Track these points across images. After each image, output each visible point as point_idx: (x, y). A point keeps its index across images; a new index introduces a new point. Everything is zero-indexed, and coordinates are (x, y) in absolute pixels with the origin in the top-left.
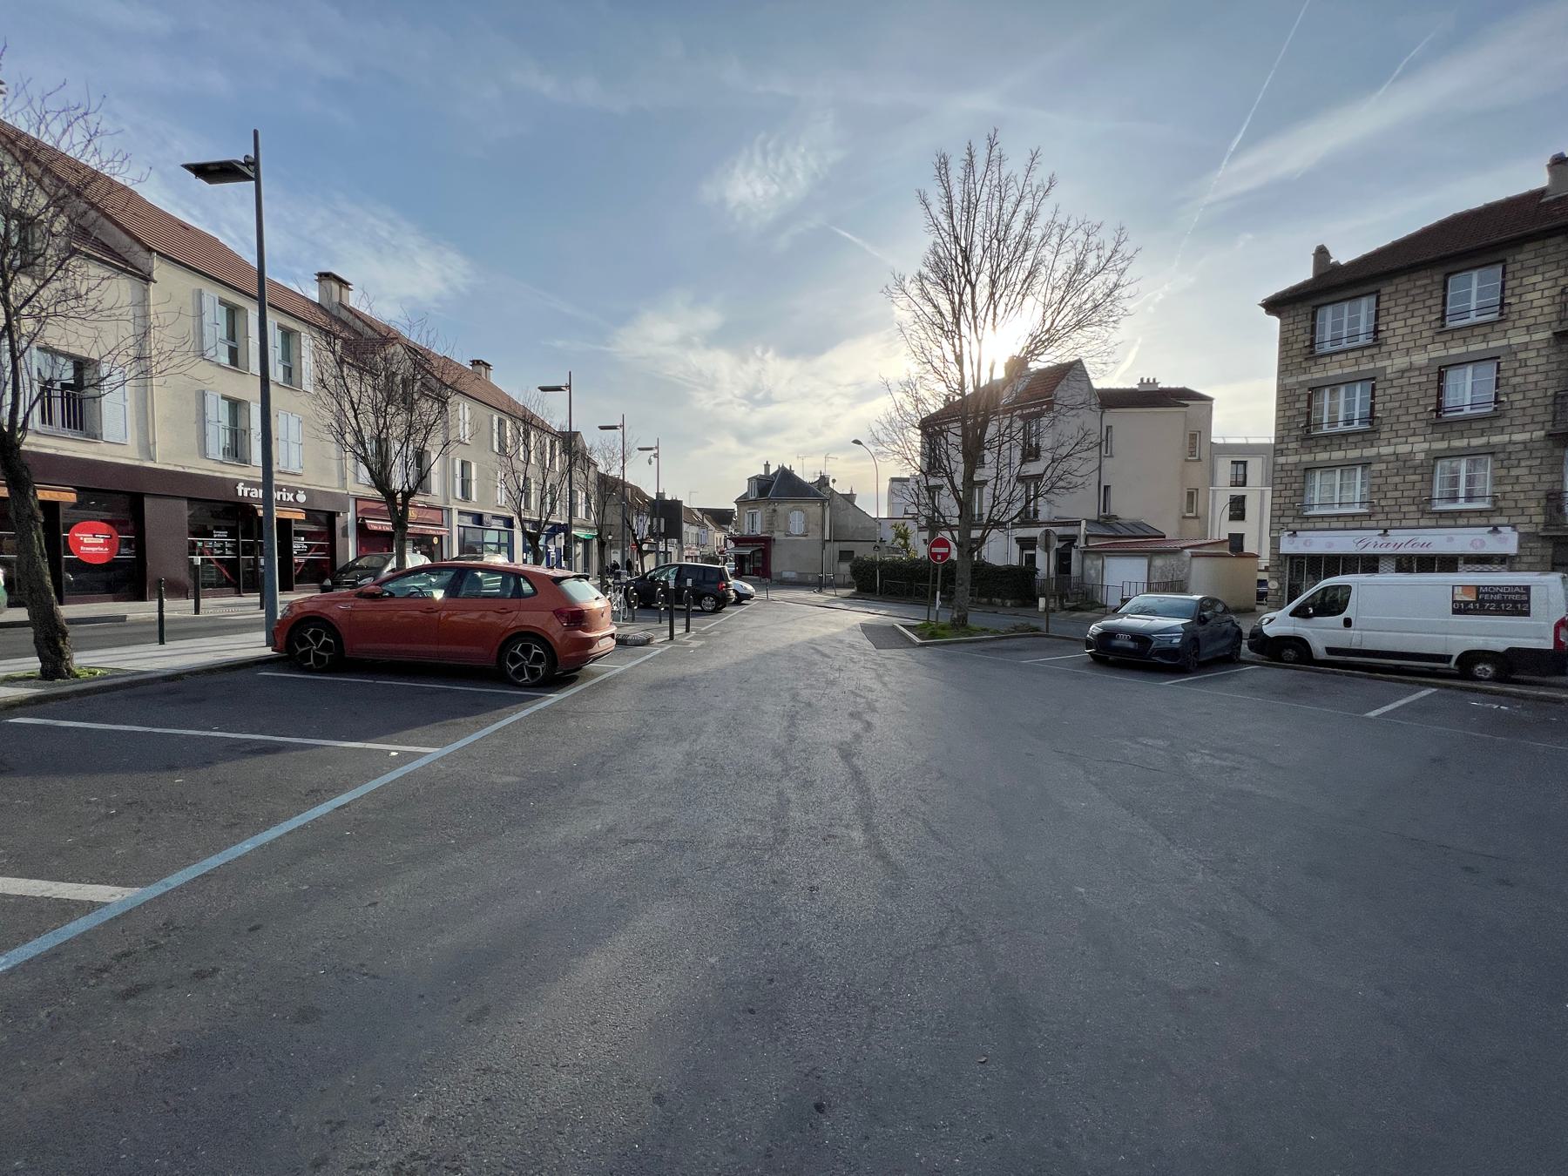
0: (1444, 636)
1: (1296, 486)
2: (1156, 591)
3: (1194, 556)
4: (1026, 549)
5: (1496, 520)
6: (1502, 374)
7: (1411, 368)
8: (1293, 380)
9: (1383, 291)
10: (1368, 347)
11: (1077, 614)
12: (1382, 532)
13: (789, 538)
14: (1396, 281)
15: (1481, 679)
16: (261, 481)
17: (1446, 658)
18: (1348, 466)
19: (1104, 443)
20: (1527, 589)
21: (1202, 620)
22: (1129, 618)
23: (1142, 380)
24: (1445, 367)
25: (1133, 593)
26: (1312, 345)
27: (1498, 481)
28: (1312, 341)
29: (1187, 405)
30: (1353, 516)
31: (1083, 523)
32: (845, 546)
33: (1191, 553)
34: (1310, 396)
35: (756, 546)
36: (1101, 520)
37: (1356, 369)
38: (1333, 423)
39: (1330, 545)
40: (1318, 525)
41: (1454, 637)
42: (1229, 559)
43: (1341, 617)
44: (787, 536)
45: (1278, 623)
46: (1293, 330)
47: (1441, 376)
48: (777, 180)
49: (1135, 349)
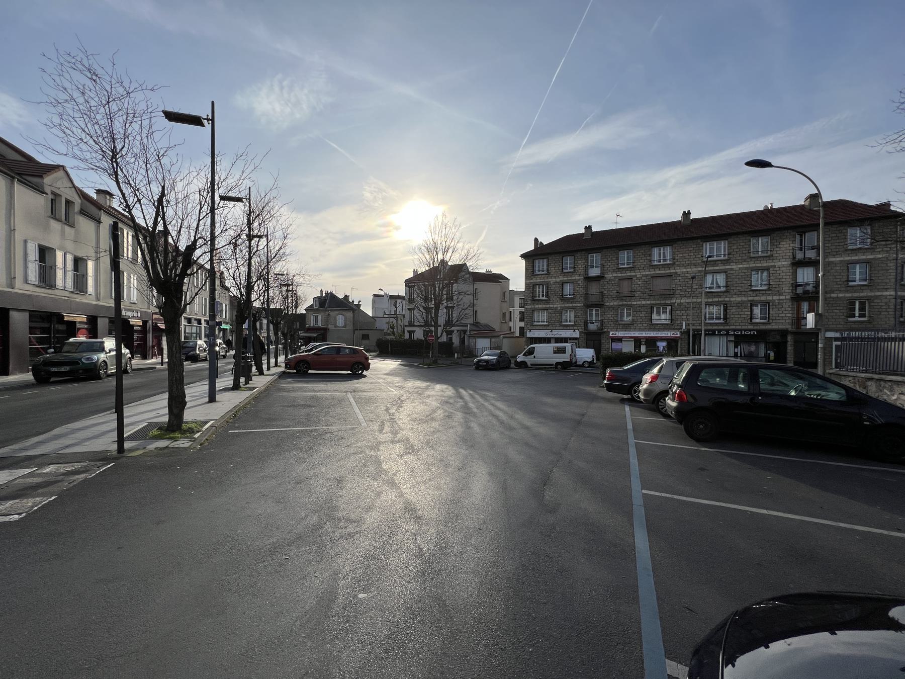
1: (530, 315)
3: (503, 338)
5: (575, 328)
8: (529, 281)
10: (547, 274)
16: (114, 306)
17: (552, 365)
19: (475, 294)
21: (501, 357)
25: (485, 350)
29: (501, 282)
31: (469, 325)
32: (365, 332)
38: (539, 296)
39: (539, 335)
43: (533, 356)
45: (521, 358)
48: (290, 105)
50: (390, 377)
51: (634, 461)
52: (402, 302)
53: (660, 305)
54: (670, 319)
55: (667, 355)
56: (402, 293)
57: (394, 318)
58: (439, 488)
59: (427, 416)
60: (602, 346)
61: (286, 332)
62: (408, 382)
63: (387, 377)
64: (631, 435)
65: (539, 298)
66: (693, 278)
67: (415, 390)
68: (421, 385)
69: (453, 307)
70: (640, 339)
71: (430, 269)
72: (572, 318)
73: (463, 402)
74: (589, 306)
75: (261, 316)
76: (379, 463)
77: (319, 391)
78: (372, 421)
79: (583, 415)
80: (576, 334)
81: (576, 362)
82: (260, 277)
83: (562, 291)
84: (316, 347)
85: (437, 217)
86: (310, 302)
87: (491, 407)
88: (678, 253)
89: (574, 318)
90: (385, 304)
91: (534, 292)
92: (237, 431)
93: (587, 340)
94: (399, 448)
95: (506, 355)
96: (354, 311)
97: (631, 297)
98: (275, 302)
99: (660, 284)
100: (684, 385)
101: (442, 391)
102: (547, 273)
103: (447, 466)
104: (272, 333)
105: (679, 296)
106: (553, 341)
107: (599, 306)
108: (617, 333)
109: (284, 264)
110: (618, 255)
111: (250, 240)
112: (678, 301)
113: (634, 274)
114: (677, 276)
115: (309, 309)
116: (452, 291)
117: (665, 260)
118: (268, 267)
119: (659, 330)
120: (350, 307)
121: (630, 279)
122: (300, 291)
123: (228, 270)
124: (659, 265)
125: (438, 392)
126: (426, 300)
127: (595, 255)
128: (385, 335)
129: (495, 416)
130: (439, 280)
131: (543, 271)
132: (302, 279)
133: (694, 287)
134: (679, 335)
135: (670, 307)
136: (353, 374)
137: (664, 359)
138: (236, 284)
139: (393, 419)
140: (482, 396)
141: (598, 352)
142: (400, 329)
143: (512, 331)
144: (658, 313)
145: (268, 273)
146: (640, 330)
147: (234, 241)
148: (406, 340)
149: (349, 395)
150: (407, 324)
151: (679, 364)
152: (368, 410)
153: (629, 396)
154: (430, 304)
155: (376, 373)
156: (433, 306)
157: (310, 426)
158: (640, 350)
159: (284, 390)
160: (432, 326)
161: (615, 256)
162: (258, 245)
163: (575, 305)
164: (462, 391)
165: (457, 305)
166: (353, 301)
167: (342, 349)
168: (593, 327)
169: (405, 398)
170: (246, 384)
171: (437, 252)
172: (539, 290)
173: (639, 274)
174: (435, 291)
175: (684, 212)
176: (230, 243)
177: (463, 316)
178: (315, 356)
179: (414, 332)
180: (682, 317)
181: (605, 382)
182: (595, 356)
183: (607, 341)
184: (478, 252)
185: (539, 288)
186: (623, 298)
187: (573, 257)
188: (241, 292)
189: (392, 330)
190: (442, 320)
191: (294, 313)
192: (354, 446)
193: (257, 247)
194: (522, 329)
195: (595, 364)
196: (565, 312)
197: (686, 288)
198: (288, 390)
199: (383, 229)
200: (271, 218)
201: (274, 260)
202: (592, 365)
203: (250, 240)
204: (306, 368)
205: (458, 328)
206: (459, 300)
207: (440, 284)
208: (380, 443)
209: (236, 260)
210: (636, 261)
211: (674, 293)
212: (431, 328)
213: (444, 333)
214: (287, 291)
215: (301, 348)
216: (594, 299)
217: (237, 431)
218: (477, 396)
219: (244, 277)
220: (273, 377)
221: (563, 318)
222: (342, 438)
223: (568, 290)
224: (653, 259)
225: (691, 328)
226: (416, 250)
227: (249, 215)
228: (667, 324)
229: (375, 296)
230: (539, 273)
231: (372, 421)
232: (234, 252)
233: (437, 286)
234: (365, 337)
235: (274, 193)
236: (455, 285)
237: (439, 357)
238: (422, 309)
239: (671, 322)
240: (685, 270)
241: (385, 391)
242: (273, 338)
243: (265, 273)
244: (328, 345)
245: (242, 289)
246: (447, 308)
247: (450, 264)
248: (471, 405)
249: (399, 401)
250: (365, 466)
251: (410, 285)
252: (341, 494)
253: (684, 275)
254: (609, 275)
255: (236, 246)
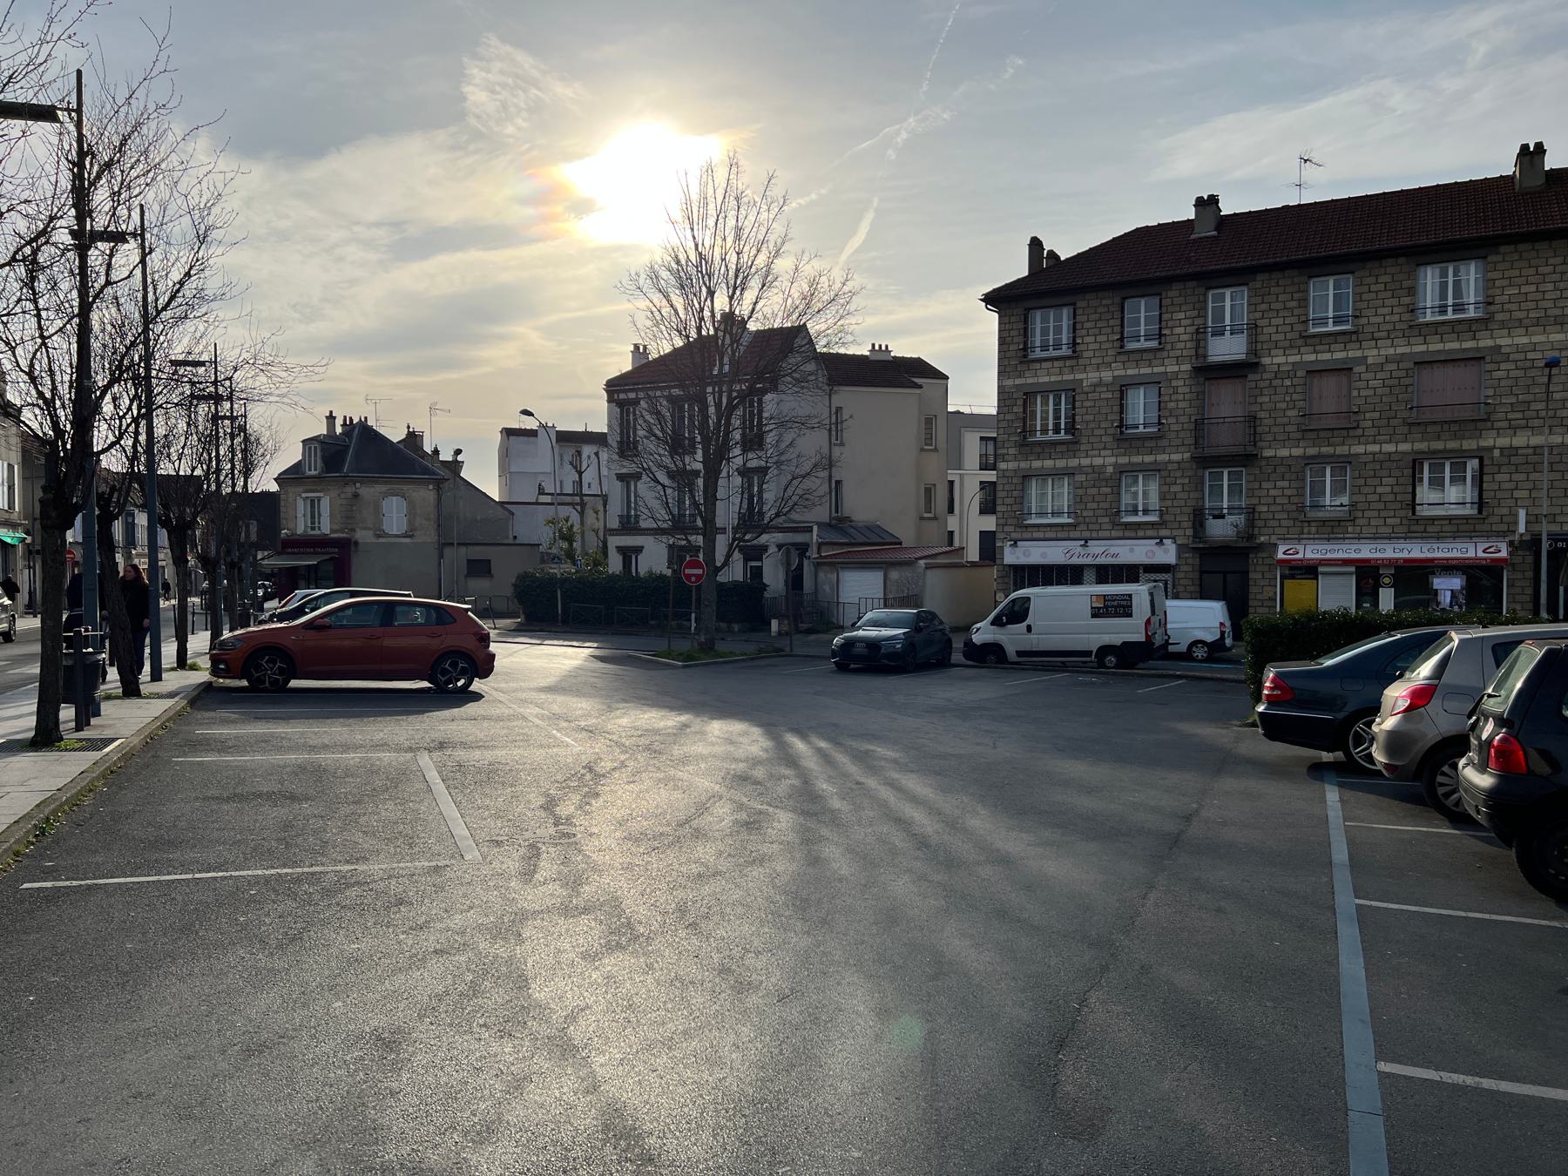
0: (1087, 636)
1: (1015, 493)
2: (892, 607)
3: (928, 567)
4: (751, 560)
5: (1164, 532)
6: (1162, 399)
7: (1100, 384)
9: (1080, 304)
11: (813, 637)
12: (1083, 542)
13: (384, 540)
14: (1088, 296)
15: (1109, 668)
17: (1088, 653)
18: (1057, 474)
19: (836, 426)
20: (1130, 596)
21: (918, 630)
22: (864, 630)
23: (873, 345)
24: (1124, 386)
25: (869, 607)
26: (1025, 349)
27: (1163, 497)
28: (1025, 343)
29: (920, 387)
30: (1062, 525)
31: (815, 528)
32: (478, 553)
33: (925, 564)
34: (1025, 401)
35: (323, 553)
36: (833, 522)
37: (1059, 378)
38: (1045, 431)
39: (1044, 555)
40: (1036, 535)
41: (1093, 636)
42: (964, 569)
43: (1025, 624)
44: (379, 536)
45: (983, 633)
46: (1009, 330)
47: (1122, 392)
49: (870, 216)
50: (560, 698)
51: (1352, 967)
52: (597, 454)
53: (1446, 454)
54: (1476, 500)
55: (1464, 620)
56: (600, 425)
57: (572, 504)
58: (714, 1062)
59: (680, 825)
60: (1253, 590)
61: (213, 553)
62: (618, 712)
63: (550, 697)
64: (1343, 880)
65: (1056, 437)
66: (1552, 364)
67: (643, 741)
68: (662, 724)
69: (763, 471)
70: (1377, 568)
71: (688, 346)
72: (1154, 501)
73: (797, 776)
74: (1207, 461)
75: (126, 500)
76: (522, 983)
77: (325, 747)
78: (498, 844)
79: (1188, 818)
80: (1167, 554)
81: (1167, 643)
82: (121, 374)
83: (1121, 413)
84: (315, 603)
85: (710, 169)
86: (291, 455)
87: (886, 793)
88: (1505, 282)
89: (1161, 500)
90: (542, 459)
91: (1026, 418)
92: (49, 884)
93: (1202, 572)
94: (588, 931)
95: (936, 622)
96: (439, 483)
97: (1349, 426)
98: (174, 457)
99: (1447, 388)
100: (1518, 719)
101: (731, 742)
102: (1069, 352)
103: (742, 987)
104: (165, 557)
105: (1505, 424)
106: (1089, 575)
107: (1245, 459)
108: (1300, 548)
109: (201, 328)
110: (1307, 291)
111: (82, 249)
112: (1503, 442)
113: (1359, 354)
114: (1499, 358)
115: (289, 478)
116: (760, 418)
117: (1459, 308)
118: (147, 340)
119: (1439, 537)
120: (426, 471)
121: (1344, 370)
122: (258, 419)
123: (13, 349)
124: (1443, 323)
125: (713, 744)
126: (678, 445)
127: (1228, 293)
128: (543, 561)
129: (900, 822)
130: (718, 381)
131: (1058, 346)
132: (262, 379)
133: (1557, 396)
134: (1504, 554)
135: (1476, 462)
136: (435, 691)
137: (1453, 634)
138: (41, 395)
139: (568, 835)
140: (861, 758)
141: (1237, 610)
142: (593, 543)
143: (957, 544)
144: (1437, 483)
145: (148, 357)
146: (1375, 537)
147: (28, 250)
148: (613, 577)
149: (425, 760)
150: (614, 523)
151: (1503, 650)
152: (488, 808)
153: (1340, 755)
154: (687, 459)
155: (513, 685)
156: (699, 466)
157: (295, 864)
158: (1376, 604)
159: (205, 745)
160: (696, 531)
161: (1296, 296)
162: (109, 266)
163: (1162, 458)
164: (799, 745)
165: (778, 463)
166: (436, 452)
167: (399, 609)
168: (1221, 530)
169: (609, 765)
170: (78, 728)
171: (709, 288)
172: (1045, 412)
173: (1372, 355)
174: (706, 417)
175: (1525, 147)
176: (14, 259)
177: (795, 498)
178: (311, 633)
179: (639, 550)
180: (1517, 494)
181: (1261, 708)
182: (1228, 624)
183: (1267, 575)
184: (846, 289)
185: (1045, 403)
186: (1322, 434)
187: (1156, 300)
188: (55, 425)
189: (565, 545)
190: (728, 512)
191: (239, 489)
192: (439, 925)
193: (107, 274)
194: (987, 539)
195: (1230, 649)
196: (1130, 481)
197: (1531, 397)
198: (222, 746)
199: (530, 211)
200: (151, 175)
201: (165, 315)
202: (1217, 655)
203: (82, 249)
204: (281, 671)
205: (780, 537)
206: (783, 446)
207: (720, 393)
208: (523, 916)
209: (38, 316)
210: (1365, 312)
211: (1489, 414)
212: (692, 538)
213: (737, 555)
214: (216, 418)
215: (267, 605)
216: (1225, 439)
217: (49, 884)
218: (841, 758)
219: (65, 378)
220: (169, 703)
221: (1123, 502)
222: (400, 902)
223: (1140, 408)
224: (1421, 305)
225: (1545, 528)
226: (641, 281)
227: (80, 164)
228: (1466, 518)
229: (509, 433)
230: (1045, 354)
231: (498, 844)
232: (30, 282)
233: (710, 399)
234: (480, 568)
235: (159, 91)
236: (768, 397)
237: (718, 630)
238: (662, 477)
239: (1480, 512)
240: (1525, 340)
241: (542, 746)
242: (169, 573)
243: (136, 358)
244: (353, 594)
245: (61, 413)
246: (744, 472)
247: (752, 326)
248: (823, 786)
249: (588, 777)
250: (475, 990)
251: (622, 396)
252: (395, 1085)
253: (1522, 356)
254: (1275, 360)
255: (34, 268)
